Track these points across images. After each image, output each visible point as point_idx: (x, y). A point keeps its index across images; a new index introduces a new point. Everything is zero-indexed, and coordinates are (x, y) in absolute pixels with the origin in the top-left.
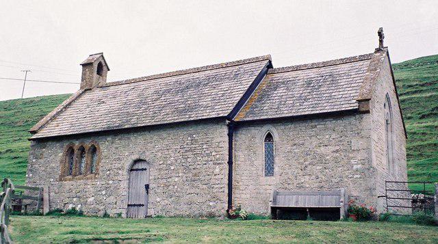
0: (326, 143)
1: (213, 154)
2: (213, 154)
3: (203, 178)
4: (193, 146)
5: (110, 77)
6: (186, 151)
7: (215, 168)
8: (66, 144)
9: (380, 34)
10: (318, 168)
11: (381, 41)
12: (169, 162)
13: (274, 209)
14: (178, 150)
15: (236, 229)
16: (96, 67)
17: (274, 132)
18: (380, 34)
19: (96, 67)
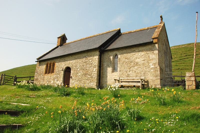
0: (139, 57)
1: (93, 63)
2: (93, 63)
3: (89, 73)
4: (86, 61)
5: (67, 42)
6: (84, 63)
7: (93, 69)
8: (46, 62)
9: (161, 17)
10: (136, 68)
11: (162, 20)
12: (77, 67)
13: (166, 105)
14: (81, 63)
15: (123, 51)
16: (63, 39)
17: (117, 53)
18: (161, 17)
19: (63, 39)
